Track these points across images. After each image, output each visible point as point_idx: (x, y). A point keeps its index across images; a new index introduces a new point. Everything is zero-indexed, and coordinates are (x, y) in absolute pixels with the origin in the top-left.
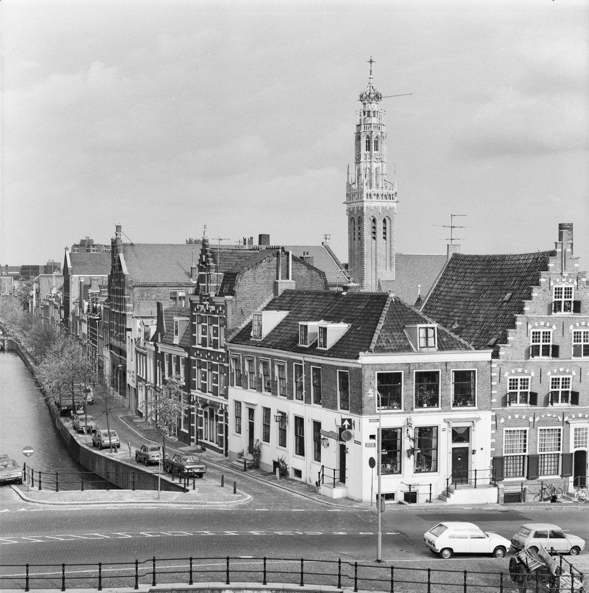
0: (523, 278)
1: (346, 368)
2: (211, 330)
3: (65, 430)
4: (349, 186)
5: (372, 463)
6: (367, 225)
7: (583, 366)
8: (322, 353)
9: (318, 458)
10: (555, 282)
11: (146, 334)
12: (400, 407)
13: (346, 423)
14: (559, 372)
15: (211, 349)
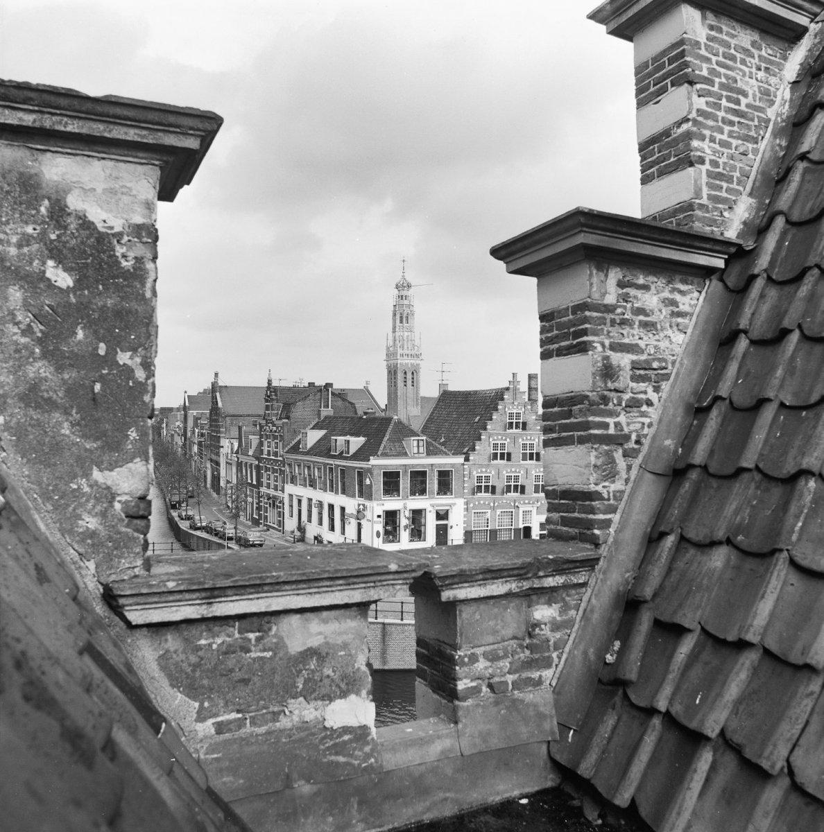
0: (488, 407)
1: (362, 468)
2: (273, 444)
3: (173, 518)
4: (388, 348)
5: (378, 534)
6: (400, 376)
7: (529, 467)
8: (346, 458)
9: (343, 533)
10: (509, 409)
11: (232, 449)
12: (399, 496)
13: (361, 507)
14: (511, 471)
15: (273, 458)
